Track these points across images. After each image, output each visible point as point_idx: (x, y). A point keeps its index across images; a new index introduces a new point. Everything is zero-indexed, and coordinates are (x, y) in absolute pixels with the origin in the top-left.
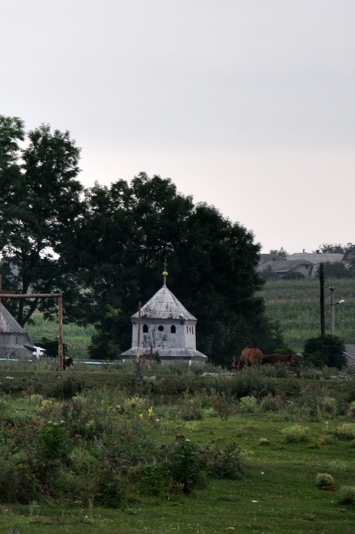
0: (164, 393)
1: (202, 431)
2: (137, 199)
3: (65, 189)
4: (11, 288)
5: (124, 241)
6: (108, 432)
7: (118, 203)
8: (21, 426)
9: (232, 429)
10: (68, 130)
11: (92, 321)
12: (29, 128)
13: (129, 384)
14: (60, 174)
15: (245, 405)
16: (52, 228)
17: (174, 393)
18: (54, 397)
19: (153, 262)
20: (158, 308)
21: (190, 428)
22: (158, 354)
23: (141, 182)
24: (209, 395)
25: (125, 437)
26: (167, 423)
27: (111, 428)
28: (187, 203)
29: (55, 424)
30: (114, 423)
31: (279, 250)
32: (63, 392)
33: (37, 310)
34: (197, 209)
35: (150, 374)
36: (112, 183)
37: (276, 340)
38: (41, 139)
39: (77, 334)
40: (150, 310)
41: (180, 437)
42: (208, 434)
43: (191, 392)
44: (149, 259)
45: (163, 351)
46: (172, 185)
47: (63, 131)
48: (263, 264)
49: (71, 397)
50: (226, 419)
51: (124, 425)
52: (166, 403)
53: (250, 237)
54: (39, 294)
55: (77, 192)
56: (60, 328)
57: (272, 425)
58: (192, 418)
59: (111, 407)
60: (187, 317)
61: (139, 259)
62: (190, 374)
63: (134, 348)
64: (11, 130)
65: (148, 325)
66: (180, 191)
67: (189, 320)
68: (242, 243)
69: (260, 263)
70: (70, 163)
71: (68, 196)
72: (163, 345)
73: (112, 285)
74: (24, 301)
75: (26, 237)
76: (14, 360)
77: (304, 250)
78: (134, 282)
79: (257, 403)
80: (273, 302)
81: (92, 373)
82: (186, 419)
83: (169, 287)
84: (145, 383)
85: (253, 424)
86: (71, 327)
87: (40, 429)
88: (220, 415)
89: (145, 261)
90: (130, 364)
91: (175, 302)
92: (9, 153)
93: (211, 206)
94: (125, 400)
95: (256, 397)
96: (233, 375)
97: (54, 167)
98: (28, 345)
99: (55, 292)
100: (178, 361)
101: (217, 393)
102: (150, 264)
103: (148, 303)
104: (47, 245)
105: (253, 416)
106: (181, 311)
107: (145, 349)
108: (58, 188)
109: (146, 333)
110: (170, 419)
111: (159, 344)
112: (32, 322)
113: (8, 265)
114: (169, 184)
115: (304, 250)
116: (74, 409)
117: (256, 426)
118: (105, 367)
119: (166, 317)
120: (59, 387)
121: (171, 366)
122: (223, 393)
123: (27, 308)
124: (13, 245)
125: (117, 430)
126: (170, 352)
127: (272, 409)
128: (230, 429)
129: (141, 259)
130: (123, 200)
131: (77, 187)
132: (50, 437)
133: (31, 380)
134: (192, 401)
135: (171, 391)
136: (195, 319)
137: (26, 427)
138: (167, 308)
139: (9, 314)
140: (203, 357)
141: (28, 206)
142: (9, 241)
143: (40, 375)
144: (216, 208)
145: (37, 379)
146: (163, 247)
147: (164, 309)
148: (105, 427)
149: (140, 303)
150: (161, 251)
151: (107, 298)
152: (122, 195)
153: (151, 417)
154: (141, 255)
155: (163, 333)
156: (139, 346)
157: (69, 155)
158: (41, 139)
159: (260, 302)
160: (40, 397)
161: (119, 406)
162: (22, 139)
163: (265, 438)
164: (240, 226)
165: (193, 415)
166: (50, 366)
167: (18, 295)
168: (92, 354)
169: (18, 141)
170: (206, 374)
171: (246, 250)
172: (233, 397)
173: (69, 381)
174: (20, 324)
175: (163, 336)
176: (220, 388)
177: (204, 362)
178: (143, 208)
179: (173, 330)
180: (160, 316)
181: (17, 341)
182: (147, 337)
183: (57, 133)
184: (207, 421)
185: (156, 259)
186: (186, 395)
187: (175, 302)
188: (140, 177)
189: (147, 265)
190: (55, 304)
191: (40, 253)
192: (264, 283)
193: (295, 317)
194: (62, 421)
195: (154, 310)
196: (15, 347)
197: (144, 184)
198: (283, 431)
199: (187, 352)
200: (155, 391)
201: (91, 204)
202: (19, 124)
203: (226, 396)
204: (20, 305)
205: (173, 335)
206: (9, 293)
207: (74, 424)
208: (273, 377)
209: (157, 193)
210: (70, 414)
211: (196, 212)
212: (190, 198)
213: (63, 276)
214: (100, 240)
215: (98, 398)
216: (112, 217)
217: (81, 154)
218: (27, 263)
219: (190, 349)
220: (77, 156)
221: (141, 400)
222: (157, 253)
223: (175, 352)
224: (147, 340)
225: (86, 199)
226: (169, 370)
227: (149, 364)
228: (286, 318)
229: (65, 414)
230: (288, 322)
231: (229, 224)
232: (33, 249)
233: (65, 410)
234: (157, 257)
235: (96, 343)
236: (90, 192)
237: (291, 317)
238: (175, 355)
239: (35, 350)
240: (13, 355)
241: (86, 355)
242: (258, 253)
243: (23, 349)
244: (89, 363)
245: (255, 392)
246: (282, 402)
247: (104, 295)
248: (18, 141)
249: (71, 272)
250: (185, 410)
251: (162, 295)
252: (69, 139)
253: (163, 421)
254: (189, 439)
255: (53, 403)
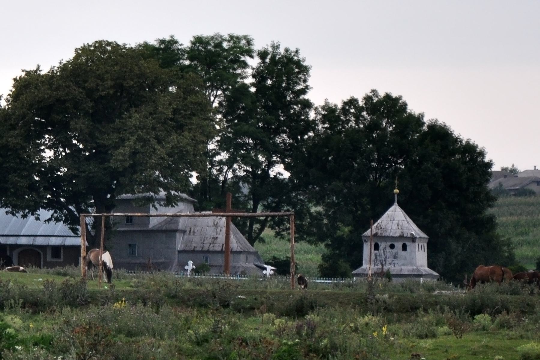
0: (397, 312)
1: (437, 349)
2: (368, 116)
3: (295, 107)
4: (241, 206)
5: (354, 159)
6: (343, 351)
7: (349, 121)
8: (255, 345)
9: (467, 347)
10: (298, 47)
11: (321, 238)
12: (257, 46)
13: (362, 302)
14: (290, 92)
15: (480, 322)
16: (282, 146)
17: (407, 311)
18: (286, 315)
19: (384, 180)
20: (389, 226)
21: (424, 346)
22: (389, 272)
23: (372, 100)
24: (443, 313)
25: (360, 355)
26: (401, 341)
27: (346, 346)
28: (418, 120)
29: (290, 343)
30: (349, 342)
31: (510, 167)
32: (296, 311)
34: (429, 127)
35: (383, 292)
36: (343, 100)
37: (507, 257)
38: (269, 57)
39: (306, 252)
40: (381, 228)
41: (416, 356)
42: (443, 352)
43: (426, 311)
44: (380, 176)
45: (394, 269)
46: (403, 103)
47: (293, 49)
48: (494, 181)
49: (304, 315)
50: (460, 337)
51: (359, 343)
52: (399, 321)
53: (482, 154)
54: (268, 213)
55: (308, 110)
56: (292, 247)
57: (508, 343)
58: (427, 336)
59: (344, 325)
60: (418, 234)
61: (370, 176)
62: (422, 292)
63: (365, 266)
64: (240, 47)
65: (379, 243)
66: (411, 109)
67: (420, 238)
68: (473, 160)
69: (491, 181)
70: (300, 80)
71: (299, 114)
72: (394, 263)
73: (342, 203)
74: (254, 220)
75: (256, 156)
76: (244, 279)
77: (535, 167)
78: (364, 200)
79: (491, 321)
80: (504, 219)
81: (323, 291)
82: (421, 337)
83: (400, 205)
84: (377, 301)
85: (488, 342)
86: (303, 245)
87: (274, 348)
88: (455, 333)
89: (376, 179)
90: (361, 282)
91: (407, 220)
92: (239, 71)
93: (443, 123)
94: (358, 318)
95: (490, 314)
96: (465, 293)
97: (284, 85)
98: (259, 264)
99: (285, 211)
100: (410, 278)
101: (451, 310)
102: (380, 182)
103: (379, 221)
104: (277, 162)
105: (488, 333)
106: (413, 229)
107: (376, 267)
108: (287, 106)
110: (404, 337)
111: (390, 262)
112: (262, 240)
113: (238, 183)
114: (400, 102)
115: (535, 167)
116: (309, 328)
117: (491, 344)
118: (336, 285)
119: (397, 235)
120: (292, 305)
121: (403, 283)
122: (457, 311)
123: (256, 226)
124: (243, 163)
125: (352, 349)
126: (401, 270)
127: (506, 326)
128: (464, 347)
129: (371, 177)
130: (354, 118)
131: (307, 105)
132: (285, 356)
133: (264, 299)
134: (425, 319)
135: (404, 309)
136: (426, 236)
137: (260, 346)
138: (398, 225)
139: (240, 233)
140: (434, 275)
141: (258, 124)
142: (239, 160)
143: (272, 294)
144: (447, 125)
145: (269, 298)
146: (393, 164)
147: (395, 227)
148: (340, 346)
149: (372, 221)
150: (392, 169)
151: (338, 216)
152: (353, 113)
153: (386, 335)
154: (372, 173)
155: (394, 251)
156: (370, 264)
157: (299, 73)
158: (269, 57)
159: (491, 219)
160: (272, 316)
161: (352, 325)
162: (252, 57)
163: (500, 356)
164: (471, 143)
165: (428, 333)
166: (280, 285)
167: (250, 214)
168: (322, 272)
169: (248, 59)
170: (438, 291)
171: (478, 167)
172: (466, 315)
173: (301, 300)
174: (250, 243)
175: (394, 254)
176: (454, 306)
177: (435, 280)
178: (374, 126)
179: (404, 248)
180: (391, 234)
181: (247, 260)
183: (287, 50)
184: (441, 339)
185: (387, 177)
186: (421, 312)
187: (407, 220)
188: (371, 95)
189: (378, 183)
190: (285, 223)
191: (270, 171)
192: (496, 200)
193: (527, 234)
194: (297, 340)
195: (385, 228)
196: (245, 265)
197: (375, 101)
198: (519, 348)
199: (418, 270)
200: (388, 310)
201: (322, 121)
202: (249, 42)
203: (460, 314)
204: (250, 224)
205: (404, 253)
206: (240, 212)
207: (308, 343)
208: (507, 294)
209: (388, 111)
210: (304, 333)
211: (427, 130)
212: (422, 115)
213: (294, 194)
214: (330, 158)
215: (331, 317)
216: (342, 135)
217: (311, 72)
218: (257, 182)
219: (422, 266)
220: (307, 74)
221: (374, 318)
222: (388, 171)
223: (406, 270)
224: (378, 258)
225: (316, 117)
226: (401, 289)
227: (381, 282)
228: (518, 235)
229: (299, 333)
230: (519, 239)
231: (461, 141)
232: (263, 167)
233: (299, 329)
234: (388, 176)
235: (326, 261)
236: (320, 110)
237: (522, 234)
238: (406, 273)
239: (265, 269)
240: (243, 274)
241: (316, 273)
242: (490, 170)
243: (253, 268)
244: (320, 281)
245: (489, 309)
246: (517, 319)
247: (334, 213)
248: (248, 59)
249: (302, 191)
250: (420, 329)
251: (393, 213)
252: (298, 57)
253: (397, 339)
254: (425, 357)
255: (286, 322)
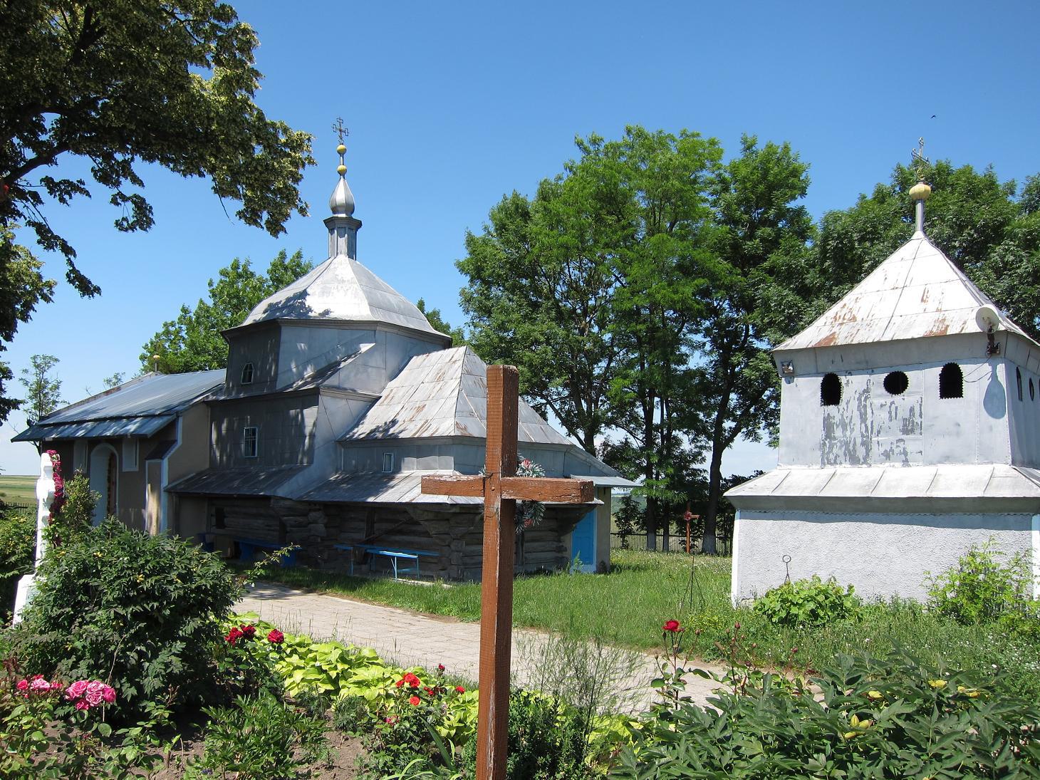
33: (474, 676)
72: (905, 453)
109: (832, 407)
175: (903, 413)
182: (837, 420)
224: (838, 433)
